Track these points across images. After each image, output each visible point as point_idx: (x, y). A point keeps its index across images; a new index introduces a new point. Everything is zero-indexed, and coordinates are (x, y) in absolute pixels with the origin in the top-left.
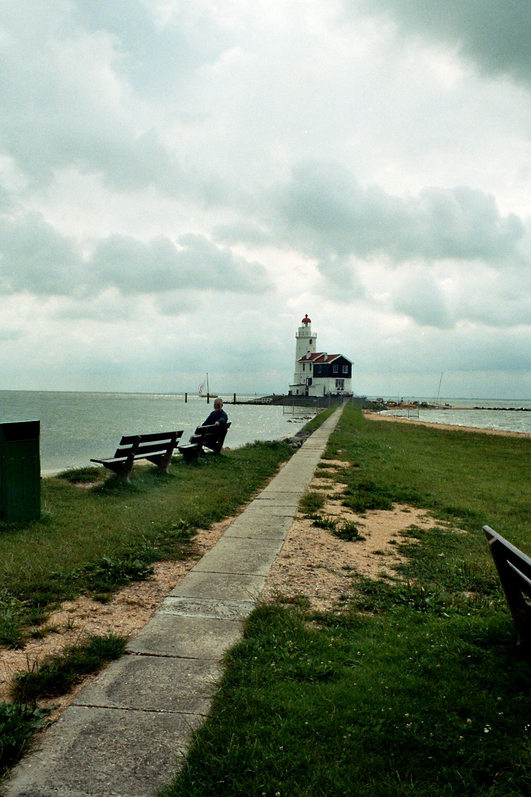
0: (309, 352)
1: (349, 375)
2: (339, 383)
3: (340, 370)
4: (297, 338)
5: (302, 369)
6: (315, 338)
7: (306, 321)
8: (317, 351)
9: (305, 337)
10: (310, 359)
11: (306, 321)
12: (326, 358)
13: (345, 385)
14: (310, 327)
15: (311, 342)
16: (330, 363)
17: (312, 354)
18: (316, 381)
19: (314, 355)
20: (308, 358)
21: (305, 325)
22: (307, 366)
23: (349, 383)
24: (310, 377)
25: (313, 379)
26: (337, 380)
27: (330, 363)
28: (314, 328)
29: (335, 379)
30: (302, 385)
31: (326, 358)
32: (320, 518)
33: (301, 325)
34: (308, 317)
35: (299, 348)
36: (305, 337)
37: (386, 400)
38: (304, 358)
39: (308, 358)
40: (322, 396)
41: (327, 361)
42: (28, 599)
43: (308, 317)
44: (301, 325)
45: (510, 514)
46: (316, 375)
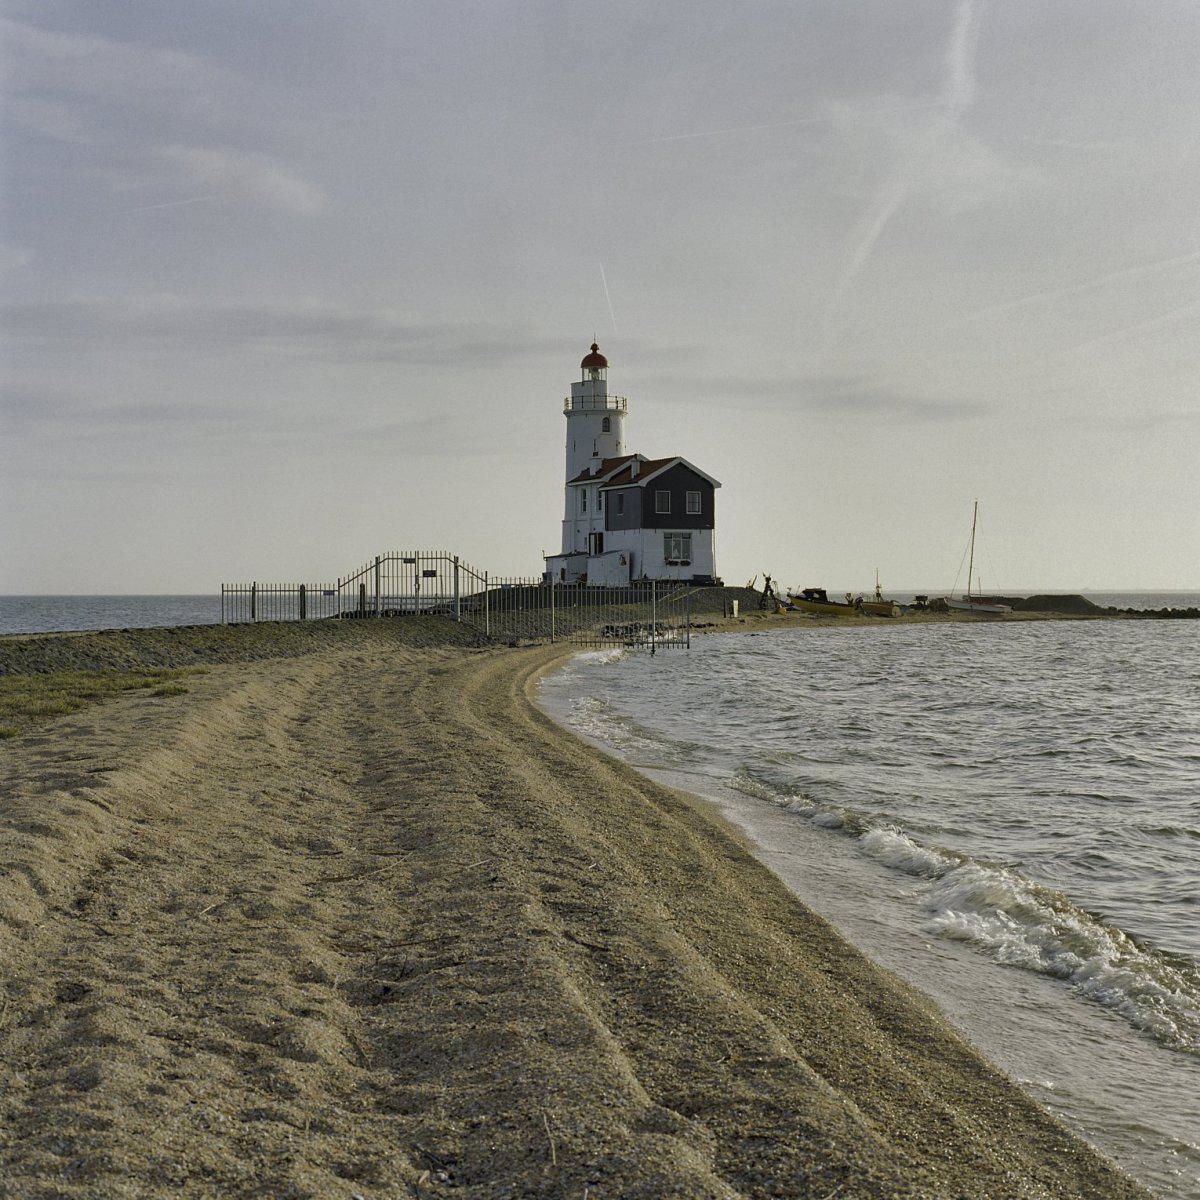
1: (706, 520)
6: (617, 412)
7: (594, 361)
8: (624, 453)
9: (591, 412)
10: (600, 473)
11: (594, 361)
12: (635, 470)
13: (696, 550)
16: (643, 483)
17: (605, 461)
19: (610, 464)
20: (592, 473)
21: (588, 376)
22: (592, 494)
23: (709, 543)
24: (598, 530)
26: (667, 537)
27: (643, 483)
28: (612, 377)
29: (660, 533)
30: (579, 554)
31: (635, 470)
33: (578, 375)
34: (598, 352)
36: (591, 412)
37: (781, 589)
38: (585, 475)
39: (592, 473)
40: (625, 583)
41: (639, 477)
42: (749, 1071)
43: (598, 352)
44: (578, 375)
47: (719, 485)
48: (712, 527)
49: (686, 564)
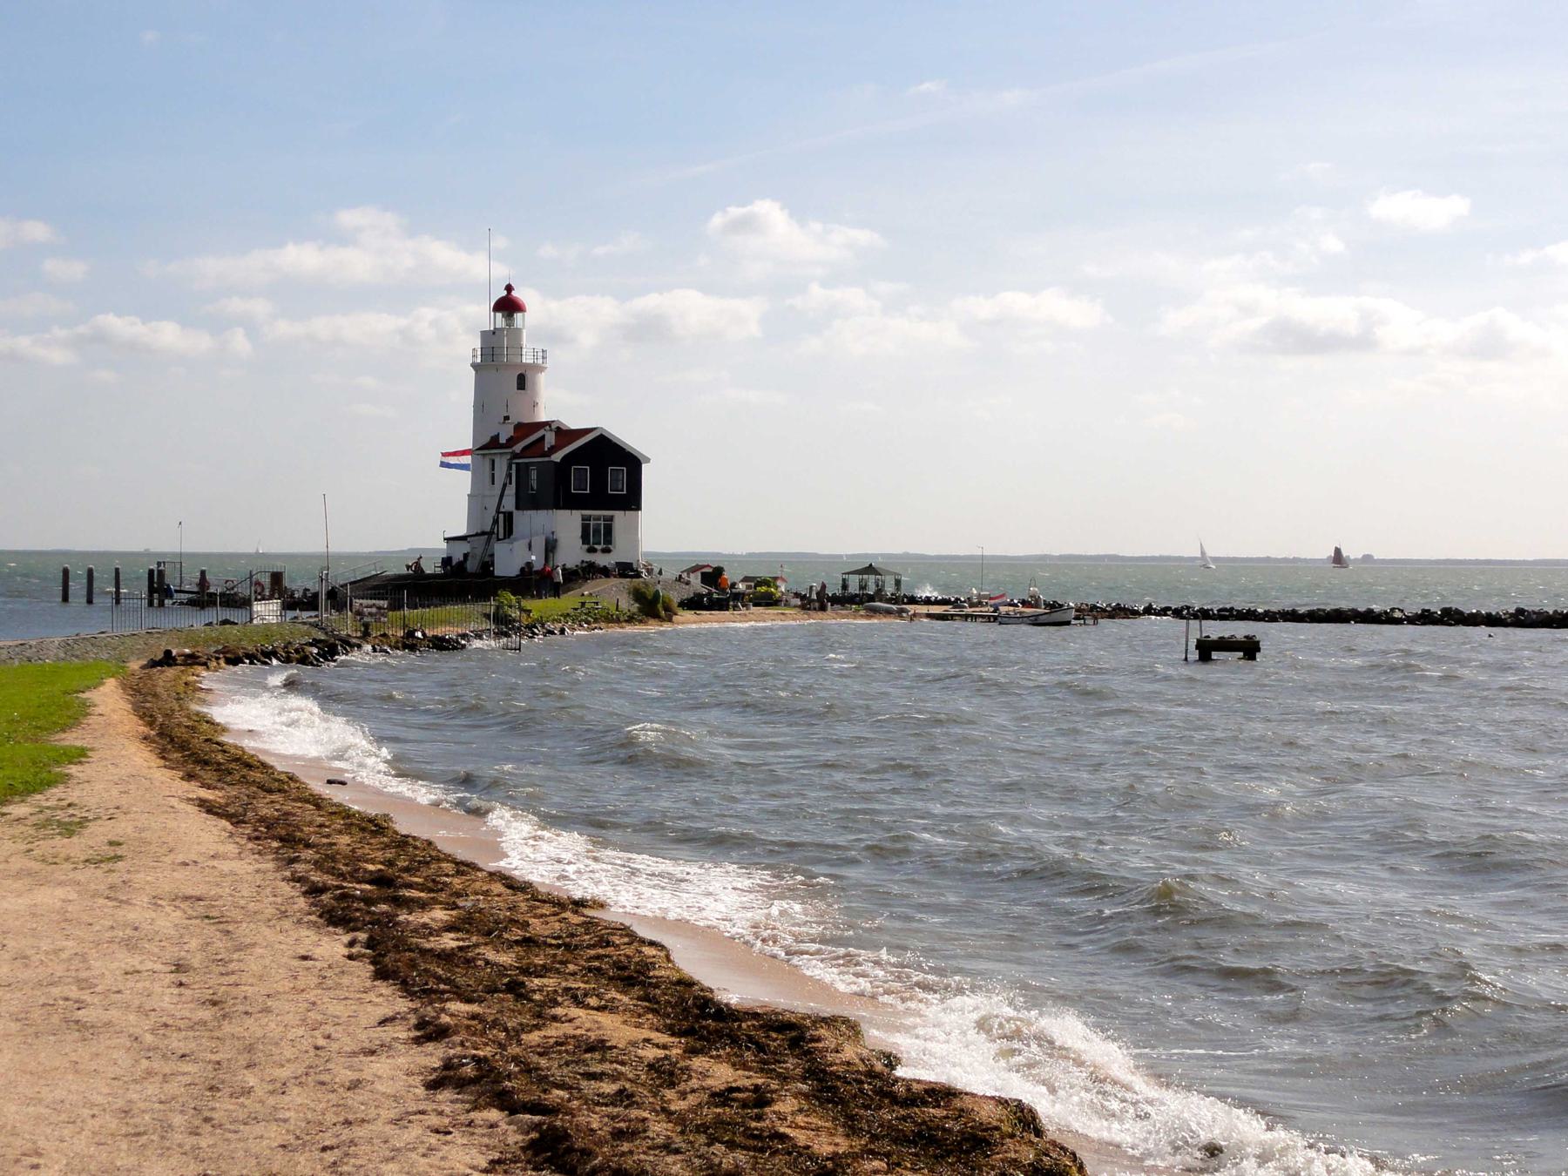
0: (507, 418)
1: (631, 500)
2: (597, 531)
3: (599, 480)
4: (474, 366)
5: (488, 479)
6: (538, 368)
8: (543, 417)
9: (501, 366)
10: (511, 442)
11: (508, 305)
14: (519, 331)
15: (522, 382)
16: (557, 457)
18: (523, 519)
19: (524, 429)
20: (503, 440)
22: (502, 465)
25: (517, 514)
31: (550, 439)
32: (1267, 1048)
35: (480, 408)
36: (501, 366)
38: (494, 443)
39: (503, 440)
41: (553, 449)
45: (254, 945)
46: (527, 501)
47: (648, 460)
48: (639, 508)
49: (607, 551)
